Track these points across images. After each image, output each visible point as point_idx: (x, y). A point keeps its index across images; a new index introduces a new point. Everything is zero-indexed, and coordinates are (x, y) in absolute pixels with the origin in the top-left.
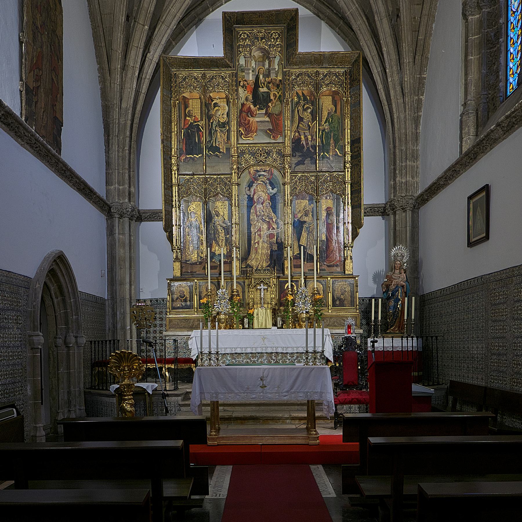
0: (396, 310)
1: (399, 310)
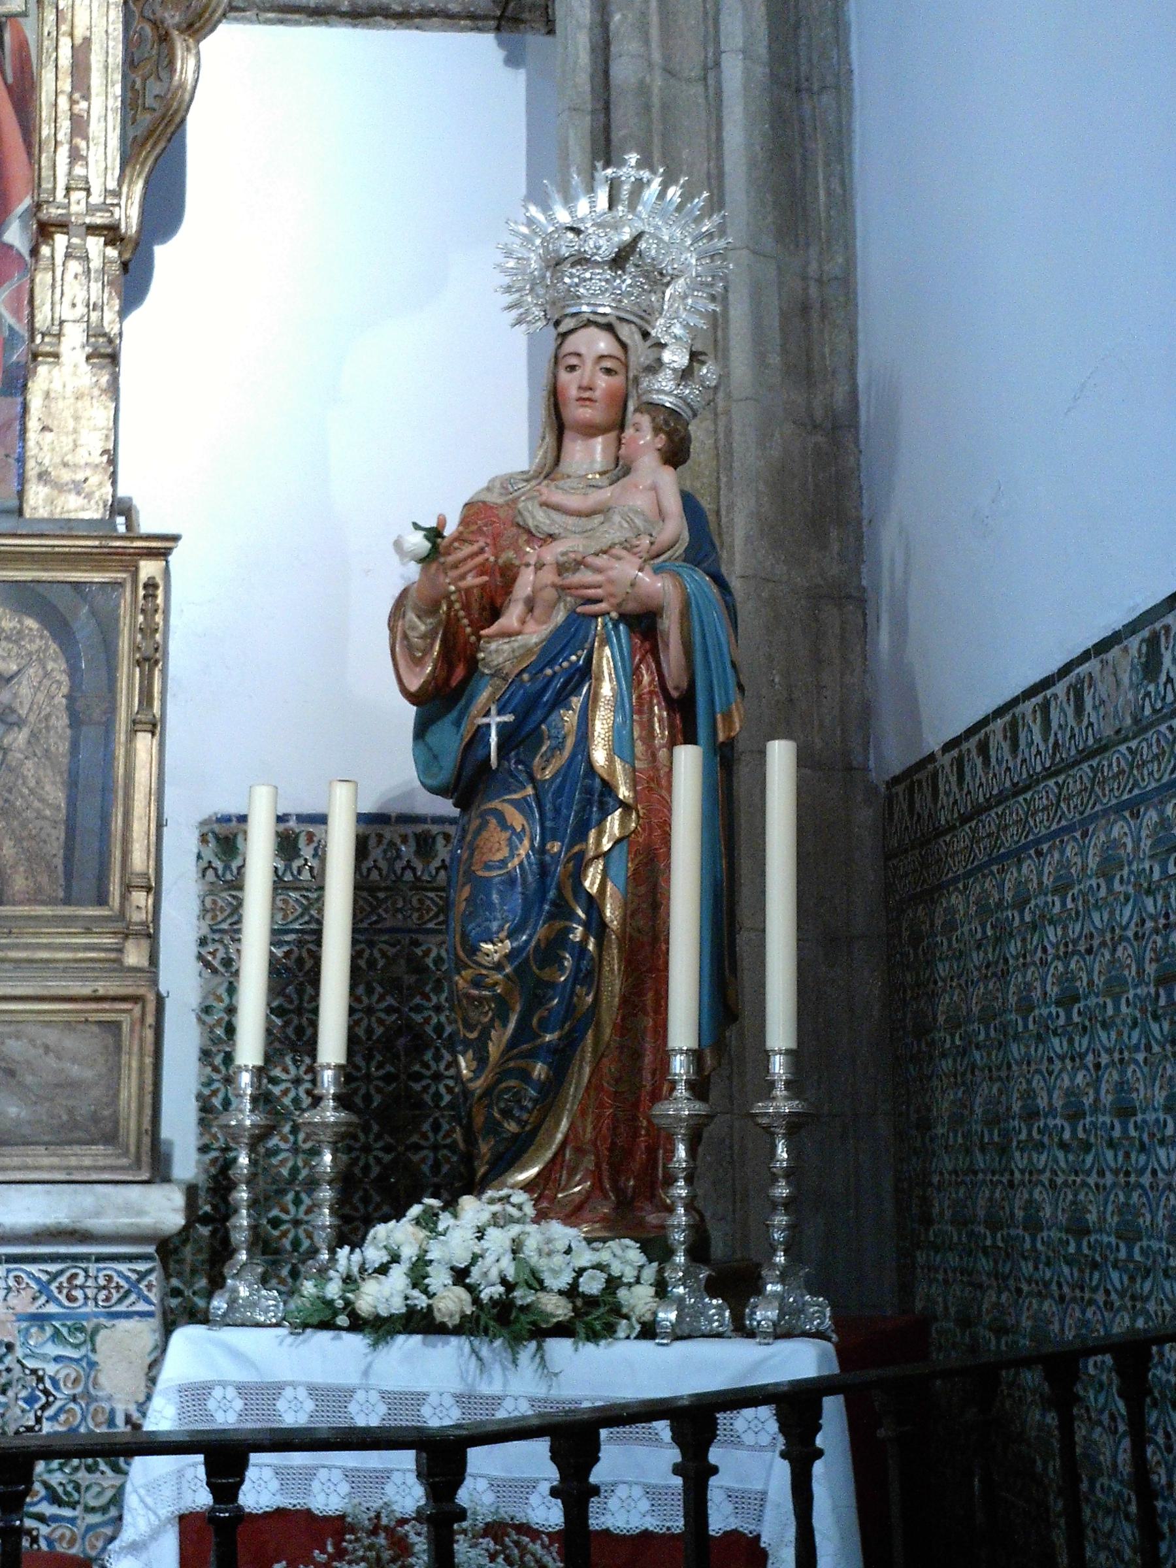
0: (560, 940)
1: (597, 925)
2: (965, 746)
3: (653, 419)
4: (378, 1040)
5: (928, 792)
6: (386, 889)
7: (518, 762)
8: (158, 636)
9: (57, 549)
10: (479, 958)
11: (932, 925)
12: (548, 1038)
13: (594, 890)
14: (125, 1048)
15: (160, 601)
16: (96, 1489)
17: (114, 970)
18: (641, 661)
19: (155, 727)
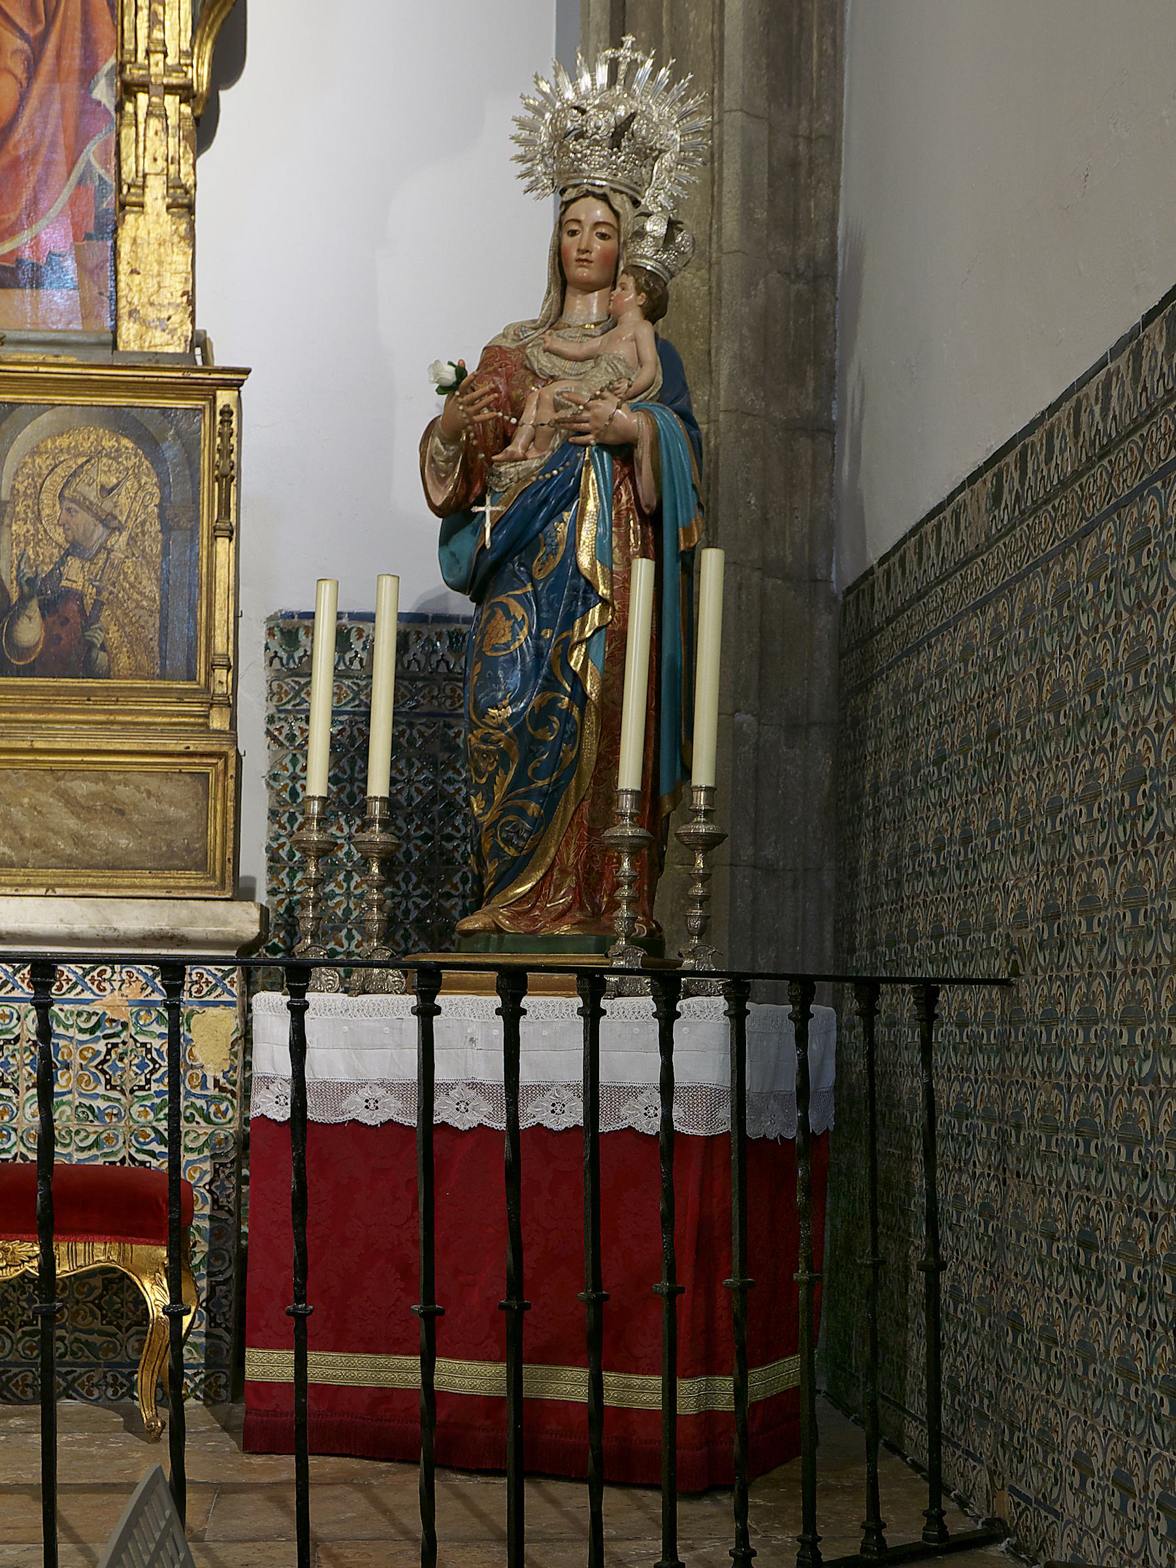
2: (892, 560)
3: (636, 280)
4: (417, 806)
5: (868, 599)
6: (424, 679)
7: (521, 564)
8: (233, 457)
9: (147, 379)
10: (487, 720)
11: (866, 711)
12: (540, 783)
13: (578, 669)
14: (212, 794)
15: (234, 425)
16: (193, 1135)
17: (202, 732)
18: (620, 483)
19: (232, 533)
